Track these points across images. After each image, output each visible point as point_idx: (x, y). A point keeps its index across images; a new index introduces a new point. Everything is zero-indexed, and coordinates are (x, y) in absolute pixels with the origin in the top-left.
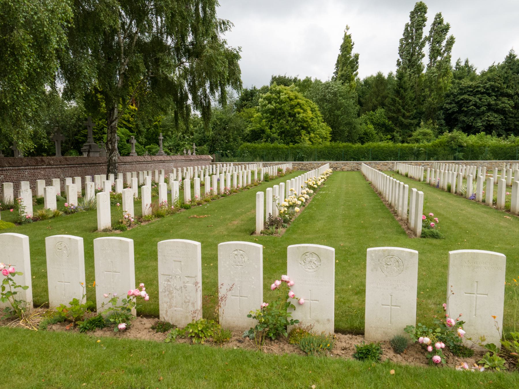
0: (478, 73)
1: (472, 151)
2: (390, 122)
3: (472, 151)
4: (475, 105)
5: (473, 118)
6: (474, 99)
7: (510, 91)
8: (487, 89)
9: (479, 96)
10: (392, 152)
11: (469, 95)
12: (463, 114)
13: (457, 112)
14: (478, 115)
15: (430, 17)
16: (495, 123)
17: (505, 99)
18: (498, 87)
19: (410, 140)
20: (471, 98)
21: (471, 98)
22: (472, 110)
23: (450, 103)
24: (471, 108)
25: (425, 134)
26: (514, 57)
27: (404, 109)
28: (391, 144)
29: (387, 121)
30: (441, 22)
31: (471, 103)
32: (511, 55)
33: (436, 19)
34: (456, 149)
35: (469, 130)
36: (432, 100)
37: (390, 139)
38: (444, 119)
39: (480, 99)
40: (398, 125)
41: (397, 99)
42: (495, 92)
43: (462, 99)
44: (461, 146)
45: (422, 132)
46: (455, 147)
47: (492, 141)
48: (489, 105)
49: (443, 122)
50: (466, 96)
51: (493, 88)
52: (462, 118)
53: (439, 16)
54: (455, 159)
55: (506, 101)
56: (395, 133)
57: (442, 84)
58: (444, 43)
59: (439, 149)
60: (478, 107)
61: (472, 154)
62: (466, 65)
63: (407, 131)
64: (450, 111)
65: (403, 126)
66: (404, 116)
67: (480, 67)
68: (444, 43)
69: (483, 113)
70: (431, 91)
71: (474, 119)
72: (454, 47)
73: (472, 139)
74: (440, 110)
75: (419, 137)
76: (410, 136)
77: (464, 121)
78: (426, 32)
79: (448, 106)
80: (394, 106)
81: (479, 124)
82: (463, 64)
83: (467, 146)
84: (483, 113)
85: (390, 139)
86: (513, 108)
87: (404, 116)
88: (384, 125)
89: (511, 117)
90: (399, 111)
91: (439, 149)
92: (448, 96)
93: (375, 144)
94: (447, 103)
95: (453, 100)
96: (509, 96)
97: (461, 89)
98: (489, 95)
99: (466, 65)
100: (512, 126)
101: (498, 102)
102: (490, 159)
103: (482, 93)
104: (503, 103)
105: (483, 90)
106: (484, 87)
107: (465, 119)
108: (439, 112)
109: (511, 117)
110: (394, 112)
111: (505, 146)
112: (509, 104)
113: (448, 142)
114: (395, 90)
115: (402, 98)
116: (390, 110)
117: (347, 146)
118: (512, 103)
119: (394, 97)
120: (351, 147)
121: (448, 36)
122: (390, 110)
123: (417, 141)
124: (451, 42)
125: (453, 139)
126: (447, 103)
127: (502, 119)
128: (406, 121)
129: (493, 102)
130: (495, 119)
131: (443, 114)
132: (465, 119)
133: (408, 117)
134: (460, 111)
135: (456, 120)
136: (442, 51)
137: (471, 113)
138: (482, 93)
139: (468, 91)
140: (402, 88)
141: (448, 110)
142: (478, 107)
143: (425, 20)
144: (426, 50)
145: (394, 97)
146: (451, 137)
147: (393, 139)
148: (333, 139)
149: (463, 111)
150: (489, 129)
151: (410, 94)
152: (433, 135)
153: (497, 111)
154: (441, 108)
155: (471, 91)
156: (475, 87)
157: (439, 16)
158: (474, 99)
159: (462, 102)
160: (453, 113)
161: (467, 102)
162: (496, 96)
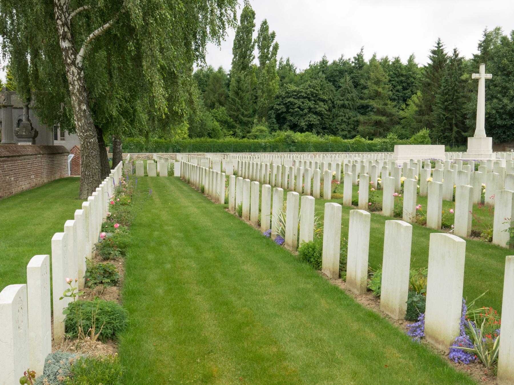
0: (298, 72)
1: (301, 146)
2: (232, 120)
3: (301, 146)
4: (299, 108)
5: (298, 118)
6: (298, 102)
7: (325, 98)
8: (308, 95)
9: (302, 100)
10: (247, 146)
11: (294, 98)
12: (290, 114)
13: (285, 112)
14: (302, 116)
15: (258, 22)
16: (314, 123)
17: (321, 104)
18: (316, 93)
19: (250, 136)
20: (296, 101)
21: (296, 101)
22: (296, 111)
23: (279, 105)
24: (296, 110)
25: (262, 131)
26: (327, 63)
27: (242, 108)
28: (233, 139)
29: (229, 118)
30: (267, 29)
31: (296, 106)
32: (324, 61)
33: (262, 26)
34: (290, 144)
35: (294, 127)
36: (263, 101)
37: (232, 135)
38: (275, 119)
39: (303, 103)
40: (238, 122)
41: (237, 99)
42: (314, 97)
43: (289, 102)
44: (293, 142)
45: (260, 130)
46: (290, 143)
47: (313, 138)
48: (310, 108)
49: (275, 121)
50: (291, 99)
51: (312, 94)
52: (289, 118)
53: (265, 23)
54: (290, 151)
55: (323, 106)
56: (236, 130)
57: (271, 87)
58: (271, 49)
59: (279, 144)
60: (302, 110)
61: (301, 148)
62: (288, 64)
63: (246, 127)
64: (280, 112)
65: (241, 123)
66: (243, 114)
67: (301, 66)
68: (271, 49)
69: (306, 115)
70: (263, 92)
71: (299, 119)
72: (279, 51)
73: (298, 137)
74: (271, 110)
75: (257, 133)
76: (249, 132)
77: (291, 120)
78: (255, 35)
79: (278, 107)
80: (235, 106)
81: (303, 124)
82: (285, 63)
83: (298, 142)
84: (306, 115)
85: (232, 135)
86: (327, 111)
87: (243, 114)
88: (226, 122)
89: (326, 118)
90: (238, 110)
91: (279, 144)
92: (278, 97)
93: (221, 140)
94: (277, 104)
95: (282, 102)
96: (323, 101)
97: (287, 92)
98: (310, 100)
99: (288, 64)
100: (328, 125)
101: (316, 106)
102: (313, 152)
103: (304, 98)
104: (320, 106)
105: (305, 95)
106: (306, 93)
107: (292, 118)
108: (270, 112)
109: (326, 118)
110: (234, 111)
111: (321, 142)
112: (324, 108)
113: (285, 139)
114: (234, 91)
115: (241, 98)
116: (231, 109)
117: (213, 141)
118: (326, 107)
119: (234, 97)
120: (216, 142)
121: (273, 44)
122: (231, 109)
123: (256, 137)
124: (276, 48)
125: (288, 136)
126: (277, 104)
127: (319, 120)
128: (245, 119)
129: (312, 106)
130: (314, 119)
131: (274, 113)
132: (292, 118)
133: (246, 116)
134: (287, 112)
135: (285, 118)
136: (269, 56)
137: (296, 114)
138: (304, 98)
139: (293, 95)
140: (241, 89)
141: (277, 110)
142: (302, 110)
143: (254, 26)
144: (256, 52)
145: (234, 97)
146: (286, 135)
147: (234, 135)
148: (190, 136)
149: (289, 112)
150: (310, 128)
151: (247, 96)
152: (267, 132)
153: (316, 113)
154: (272, 108)
155: (296, 95)
156: (299, 91)
157: (265, 23)
158: (298, 102)
159: (289, 104)
160: (282, 113)
161: (291, 103)
162: (314, 101)
